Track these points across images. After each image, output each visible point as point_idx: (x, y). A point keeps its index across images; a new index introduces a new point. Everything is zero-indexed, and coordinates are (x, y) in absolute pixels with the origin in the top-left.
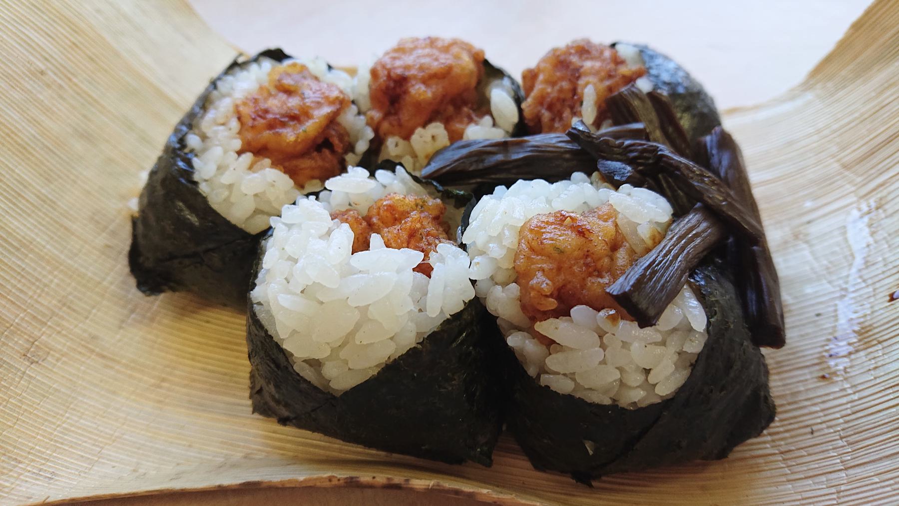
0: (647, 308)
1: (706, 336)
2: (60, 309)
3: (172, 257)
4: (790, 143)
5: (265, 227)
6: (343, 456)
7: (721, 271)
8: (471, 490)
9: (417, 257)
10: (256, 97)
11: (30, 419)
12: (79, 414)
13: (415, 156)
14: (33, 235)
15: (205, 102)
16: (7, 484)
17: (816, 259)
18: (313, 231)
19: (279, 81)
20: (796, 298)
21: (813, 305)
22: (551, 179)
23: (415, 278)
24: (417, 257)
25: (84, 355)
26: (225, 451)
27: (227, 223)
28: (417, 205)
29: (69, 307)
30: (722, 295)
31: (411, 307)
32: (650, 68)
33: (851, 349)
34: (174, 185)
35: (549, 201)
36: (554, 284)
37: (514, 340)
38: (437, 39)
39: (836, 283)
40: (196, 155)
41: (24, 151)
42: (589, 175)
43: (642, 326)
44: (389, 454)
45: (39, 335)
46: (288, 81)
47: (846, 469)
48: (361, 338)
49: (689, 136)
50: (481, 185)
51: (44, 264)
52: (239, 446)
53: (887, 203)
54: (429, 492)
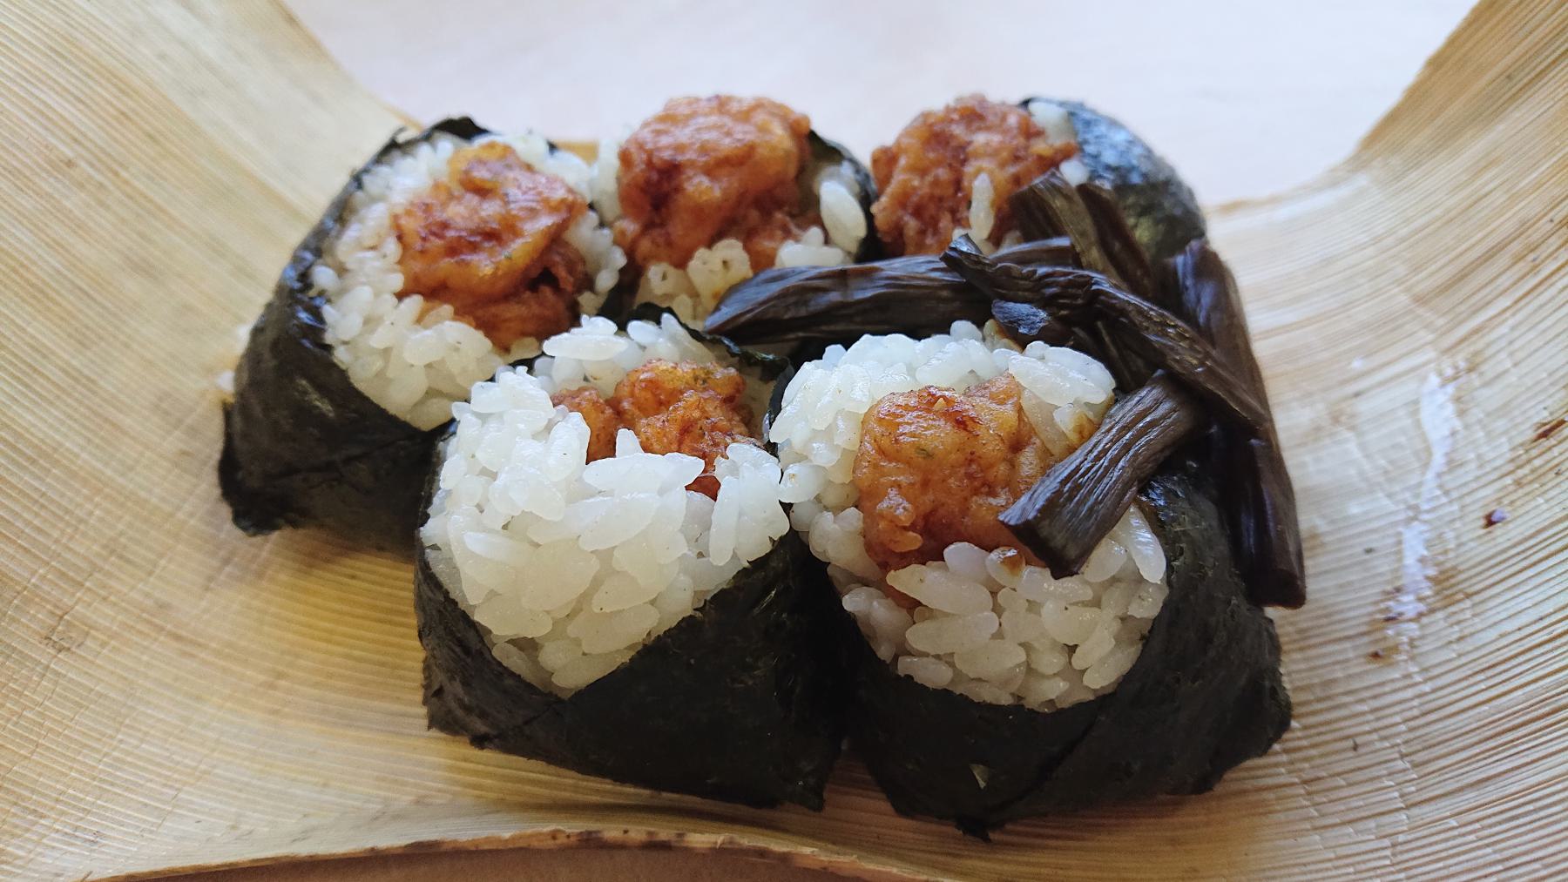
0: (1064, 547)
1: (1167, 591)
2: (105, 560)
3: (290, 471)
4: (1328, 261)
5: (444, 419)
6: (580, 798)
7: (1196, 483)
8: (785, 849)
9: (693, 467)
10: (429, 201)
11: (58, 744)
12: (140, 735)
13: (694, 294)
14: (58, 437)
15: (342, 211)
16: (21, 853)
17: (1367, 456)
18: (521, 426)
19: (467, 172)
20: (1333, 522)
21: (1359, 535)
22: (917, 333)
23: (689, 500)
24: (693, 467)
25: (148, 635)
26: (382, 793)
27: (382, 413)
28: (696, 379)
29: (121, 557)
30: (1193, 522)
31: (683, 548)
32: (1086, 142)
33: (1422, 607)
34: (291, 348)
35: (911, 370)
36: (916, 508)
37: (852, 602)
38: (729, 99)
39: (1400, 497)
40: (329, 301)
41: (40, 296)
42: (980, 325)
43: (1056, 576)
44: (655, 793)
45: (71, 603)
46: (481, 174)
47: (1408, 808)
48: (603, 602)
49: (1147, 256)
50: (805, 342)
51: (77, 485)
52: (404, 784)
53: (1486, 360)
54: (718, 852)
